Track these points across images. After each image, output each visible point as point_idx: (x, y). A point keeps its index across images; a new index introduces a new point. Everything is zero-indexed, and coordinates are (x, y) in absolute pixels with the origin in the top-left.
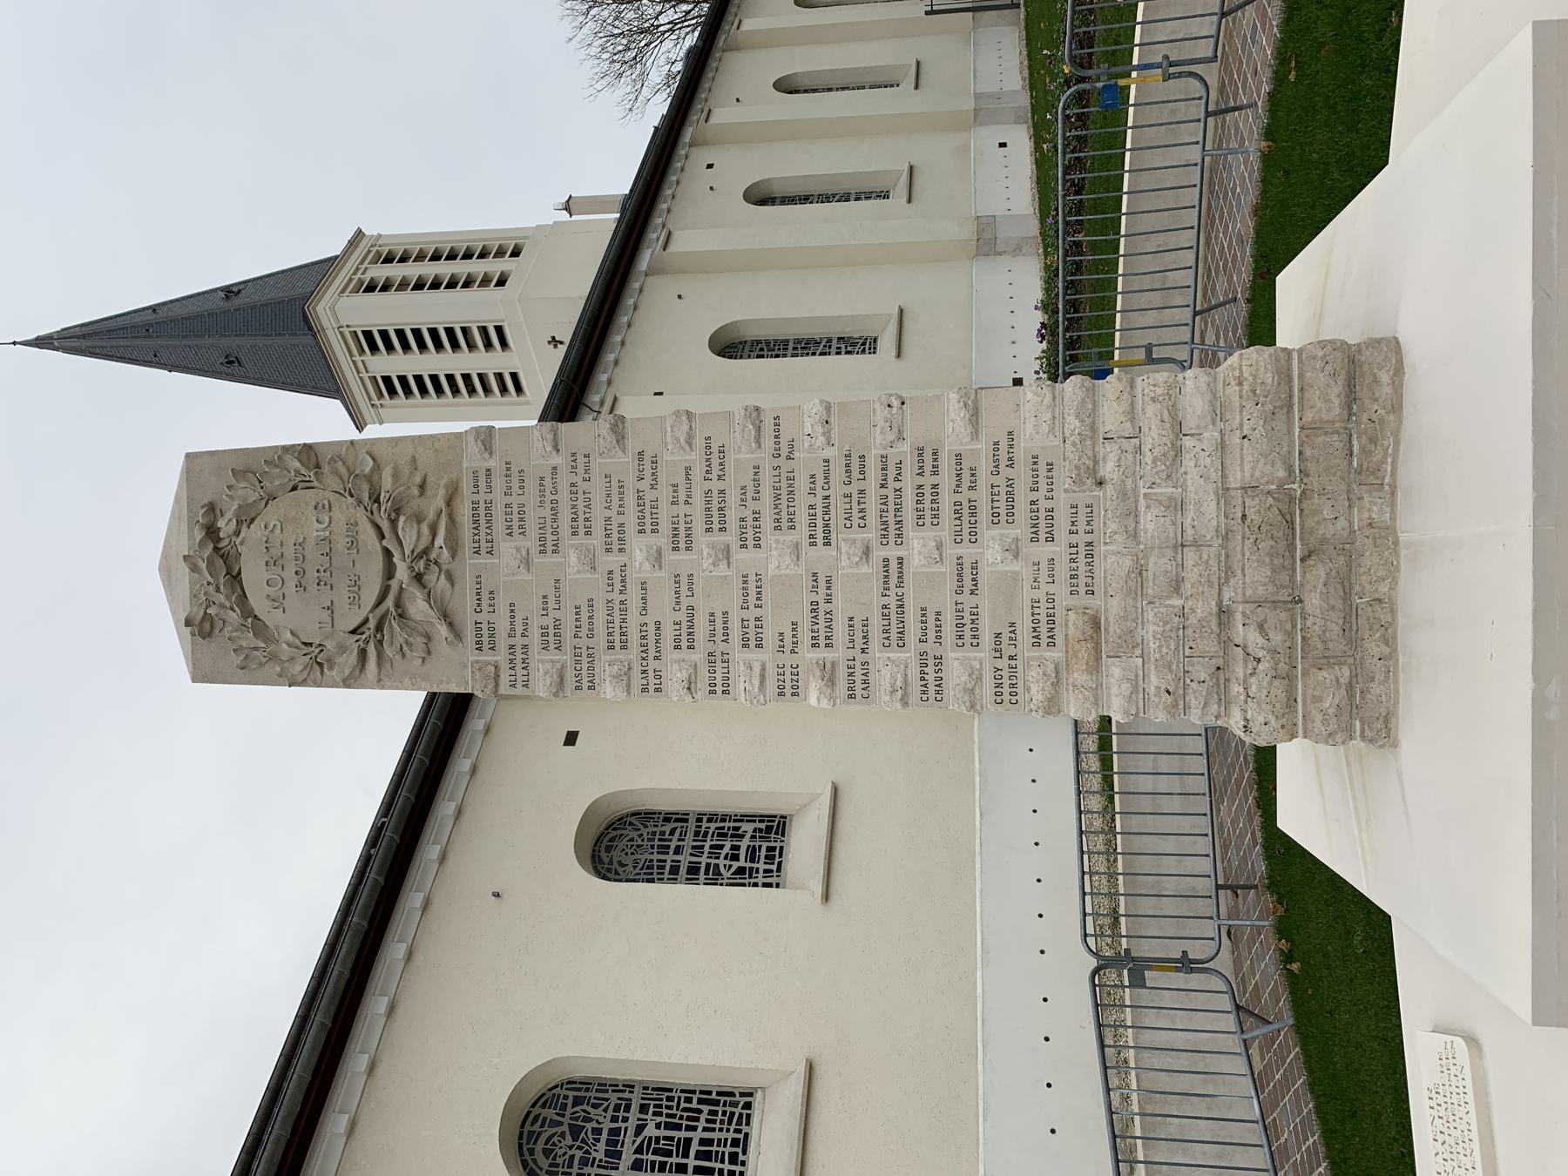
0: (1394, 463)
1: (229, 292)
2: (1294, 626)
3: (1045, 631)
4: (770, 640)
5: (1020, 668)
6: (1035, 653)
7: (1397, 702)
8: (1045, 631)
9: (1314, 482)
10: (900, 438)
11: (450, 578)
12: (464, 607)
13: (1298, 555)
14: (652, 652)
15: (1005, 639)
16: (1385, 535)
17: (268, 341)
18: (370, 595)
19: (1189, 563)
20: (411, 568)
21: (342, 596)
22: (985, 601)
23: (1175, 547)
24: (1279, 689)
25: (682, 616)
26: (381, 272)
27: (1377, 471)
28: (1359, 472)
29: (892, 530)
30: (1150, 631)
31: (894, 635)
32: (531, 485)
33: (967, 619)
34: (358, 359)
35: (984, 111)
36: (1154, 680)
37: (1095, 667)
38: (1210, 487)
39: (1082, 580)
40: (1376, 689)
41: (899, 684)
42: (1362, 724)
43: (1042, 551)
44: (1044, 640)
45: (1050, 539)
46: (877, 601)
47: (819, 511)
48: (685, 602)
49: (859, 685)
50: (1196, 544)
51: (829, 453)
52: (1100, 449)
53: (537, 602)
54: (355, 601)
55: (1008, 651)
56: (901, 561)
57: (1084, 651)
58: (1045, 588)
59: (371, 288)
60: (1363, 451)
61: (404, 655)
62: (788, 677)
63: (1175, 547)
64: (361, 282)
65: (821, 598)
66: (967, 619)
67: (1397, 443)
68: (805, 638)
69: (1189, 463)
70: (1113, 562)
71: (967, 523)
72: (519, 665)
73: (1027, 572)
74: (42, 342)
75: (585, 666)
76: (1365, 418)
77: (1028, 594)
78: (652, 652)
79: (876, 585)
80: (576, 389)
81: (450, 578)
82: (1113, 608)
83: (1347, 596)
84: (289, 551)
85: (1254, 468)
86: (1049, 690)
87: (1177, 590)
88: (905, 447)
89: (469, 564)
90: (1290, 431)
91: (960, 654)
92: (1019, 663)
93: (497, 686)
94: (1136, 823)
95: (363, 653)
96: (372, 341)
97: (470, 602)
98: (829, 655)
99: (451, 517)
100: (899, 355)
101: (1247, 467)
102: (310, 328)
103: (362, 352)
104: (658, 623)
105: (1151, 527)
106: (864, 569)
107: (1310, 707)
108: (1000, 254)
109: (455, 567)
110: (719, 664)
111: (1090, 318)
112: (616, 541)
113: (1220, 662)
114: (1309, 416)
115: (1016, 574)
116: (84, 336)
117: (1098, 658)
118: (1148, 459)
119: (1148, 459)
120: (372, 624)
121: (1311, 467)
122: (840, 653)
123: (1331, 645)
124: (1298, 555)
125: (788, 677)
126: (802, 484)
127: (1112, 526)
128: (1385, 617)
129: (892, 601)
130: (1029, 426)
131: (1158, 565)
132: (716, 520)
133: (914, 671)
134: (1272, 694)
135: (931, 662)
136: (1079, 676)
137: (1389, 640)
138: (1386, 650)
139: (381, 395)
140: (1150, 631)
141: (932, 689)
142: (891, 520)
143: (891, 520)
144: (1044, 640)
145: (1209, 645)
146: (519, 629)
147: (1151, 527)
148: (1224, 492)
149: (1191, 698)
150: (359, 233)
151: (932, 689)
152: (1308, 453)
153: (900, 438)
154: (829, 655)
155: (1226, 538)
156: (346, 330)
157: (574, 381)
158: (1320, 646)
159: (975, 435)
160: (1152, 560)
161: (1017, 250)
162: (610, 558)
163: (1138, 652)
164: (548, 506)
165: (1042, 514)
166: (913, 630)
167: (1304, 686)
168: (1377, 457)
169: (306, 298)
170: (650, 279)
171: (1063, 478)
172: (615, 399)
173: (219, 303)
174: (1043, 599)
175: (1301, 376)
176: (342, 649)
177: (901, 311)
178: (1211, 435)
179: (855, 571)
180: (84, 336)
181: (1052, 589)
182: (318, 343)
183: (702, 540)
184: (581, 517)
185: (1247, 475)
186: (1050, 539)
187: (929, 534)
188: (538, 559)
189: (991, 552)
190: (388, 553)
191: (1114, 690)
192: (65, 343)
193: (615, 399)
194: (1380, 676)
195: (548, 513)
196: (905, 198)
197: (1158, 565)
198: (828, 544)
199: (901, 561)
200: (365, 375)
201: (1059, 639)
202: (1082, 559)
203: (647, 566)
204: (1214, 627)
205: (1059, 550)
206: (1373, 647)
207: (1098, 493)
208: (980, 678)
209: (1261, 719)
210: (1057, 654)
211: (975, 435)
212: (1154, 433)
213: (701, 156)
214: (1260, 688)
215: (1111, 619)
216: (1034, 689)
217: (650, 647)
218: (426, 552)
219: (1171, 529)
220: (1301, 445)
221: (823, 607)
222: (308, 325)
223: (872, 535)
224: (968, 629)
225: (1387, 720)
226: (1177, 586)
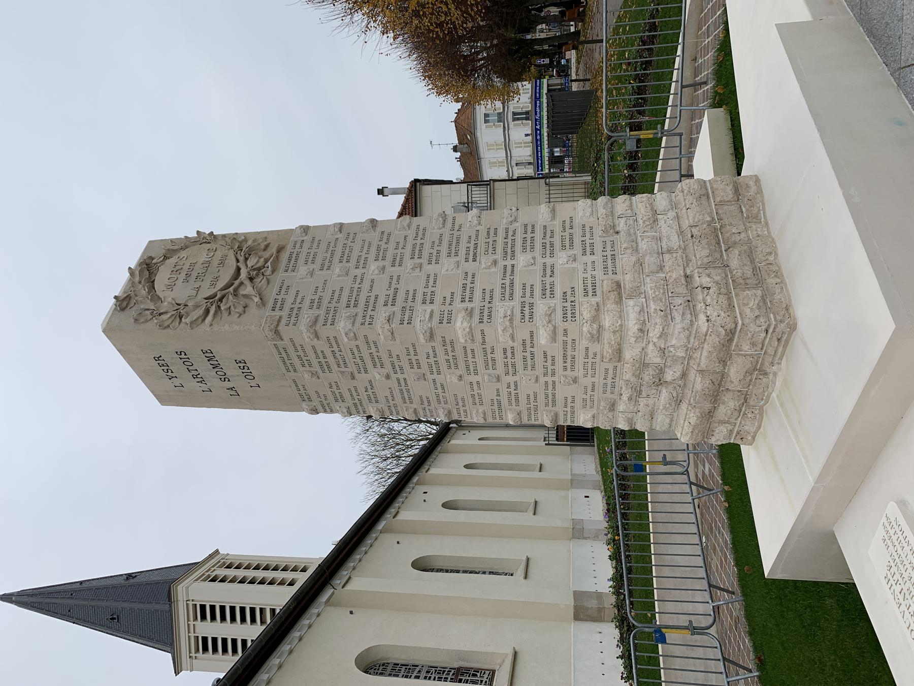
0: (764, 213)
1: (129, 576)
2: (727, 276)
3: (591, 289)
4: (438, 299)
5: (577, 306)
6: (586, 299)
7: (790, 300)
8: (591, 289)
9: (726, 221)
10: (516, 220)
11: (268, 281)
12: (271, 293)
13: (723, 249)
14: (371, 308)
15: (569, 294)
16: (769, 240)
17: (141, 606)
18: (221, 284)
19: (666, 260)
20: (249, 273)
21: (206, 284)
22: (557, 280)
23: (658, 253)
24: (723, 300)
25: (391, 292)
26: (222, 572)
27: (756, 216)
28: (748, 217)
29: (510, 253)
30: (649, 286)
31: (507, 293)
32: (323, 246)
33: (548, 287)
34: (192, 623)
35: (578, 532)
36: (653, 306)
37: (619, 301)
38: (674, 231)
39: (610, 269)
40: (777, 297)
41: (509, 313)
42: (774, 315)
43: (589, 259)
44: (590, 293)
45: (592, 253)
46: (499, 282)
47: (472, 249)
48: (393, 286)
49: (485, 318)
50: (669, 251)
51: (479, 228)
52: (617, 222)
53: (313, 289)
54: (213, 285)
55: (569, 298)
56: (513, 266)
57: (613, 296)
58: (590, 273)
59: (213, 580)
60: (747, 210)
61: (230, 313)
62: (446, 315)
63: (658, 253)
64: (209, 576)
65: (468, 282)
66: (548, 287)
67: (763, 205)
68: (458, 298)
69: (661, 223)
70: (626, 260)
71: (549, 249)
72: (294, 315)
73: (581, 268)
74: (7, 598)
75: (331, 315)
76: (746, 199)
77: (581, 275)
78: (371, 308)
79: (500, 275)
80: (327, 573)
81: (268, 281)
82: (628, 280)
83: (752, 261)
84: (186, 267)
85: (694, 218)
86: (593, 312)
87: (661, 269)
88: (515, 225)
89: (280, 275)
90: (710, 206)
91: (544, 301)
92: (577, 304)
93: (278, 325)
94: (659, 507)
95: (207, 311)
96: (205, 612)
97: (276, 290)
98: (470, 305)
99: (277, 257)
100: (526, 577)
101: (690, 218)
102: (170, 600)
103: (196, 619)
104: (376, 297)
105: (645, 247)
106: (493, 270)
107: (742, 308)
108: (586, 538)
109: (272, 278)
110: (408, 311)
111: (633, 525)
112: (362, 263)
113: (689, 298)
114: (718, 199)
115: (574, 269)
116: (32, 596)
117: (620, 298)
118: (641, 222)
119: (641, 222)
120: (219, 296)
121: (723, 216)
122: (477, 303)
123: (748, 281)
124: (723, 249)
125: (446, 315)
126: (464, 240)
127: (624, 246)
128: (774, 268)
129: (507, 282)
130: (581, 214)
131: (650, 261)
132: (417, 252)
133: (517, 312)
134: (720, 302)
135: (527, 306)
136: (611, 306)
137: (778, 274)
138: (779, 280)
139: (197, 651)
140: (649, 286)
141: (527, 317)
142: (509, 251)
143: (509, 251)
144: (590, 293)
145: (682, 290)
146: (298, 300)
147: (645, 247)
148: (681, 233)
149: (675, 314)
150: (217, 551)
151: (527, 317)
152: (720, 212)
153: (516, 220)
154: (470, 305)
155: (685, 249)
156: (191, 603)
157: (328, 568)
158: (742, 281)
159: (553, 218)
160: (647, 258)
161: (596, 537)
162: (357, 270)
163: (643, 296)
164: (330, 252)
165: (588, 245)
166: (518, 292)
167: (737, 300)
168: (755, 210)
169: (174, 580)
170: (382, 535)
171: (598, 232)
172: (350, 578)
173: (121, 581)
174: (589, 277)
175: (712, 188)
176: (197, 306)
177: (528, 559)
178: (671, 214)
179: (488, 271)
180: (32, 596)
181: (594, 273)
182: (171, 611)
183: (409, 263)
184: (346, 255)
185: (691, 221)
186: (592, 253)
187: (529, 256)
188: (318, 272)
189: (561, 258)
190: (238, 269)
191: (631, 311)
192: (19, 599)
193: (350, 578)
194: (778, 291)
195: (329, 255)
196: (532, 512)
197: (650, 261)
198: (474, 260)
199: (513, 266)
200: (192, 635)
201: (598, 292)
202: (609, 261)
203: (376, 272)
204: (684, 282)
205: (598, 258)
206: (771, 281)
207: (616, 236)
208: (554, 310)
209: (715, 314)
210: (598, 299)
211: (553, 218)
212: (643, 211)
213: (421, 489)
214: (712, 299)
215: (627, 283)
216: (585, 313)
217: (371, 304)
218: (259, 269)
219: (656, 247)
220: (717, 210)
221: (469, 285)
222: (169, 598)
223: (499, 255)
224: (548, 291)
225: (787, 309)
226: (661, 268)
